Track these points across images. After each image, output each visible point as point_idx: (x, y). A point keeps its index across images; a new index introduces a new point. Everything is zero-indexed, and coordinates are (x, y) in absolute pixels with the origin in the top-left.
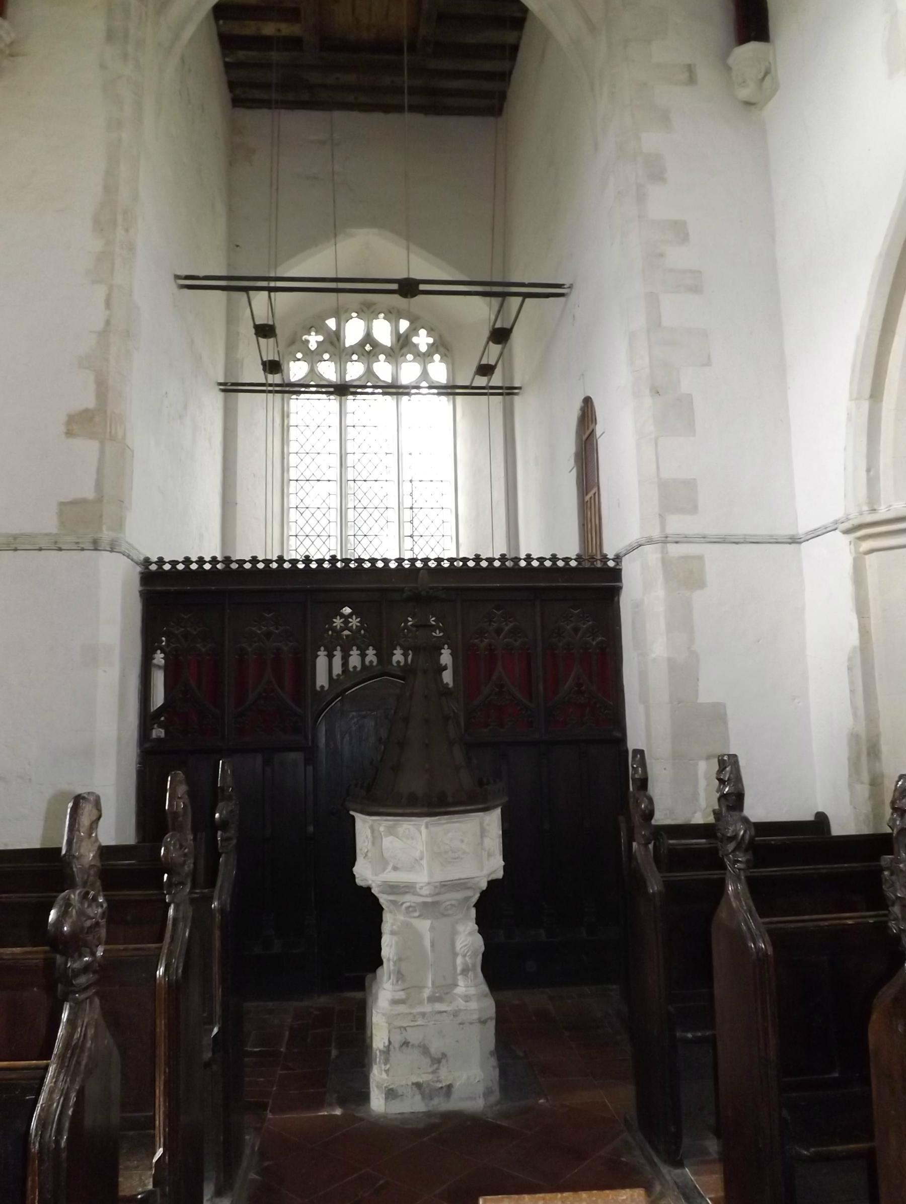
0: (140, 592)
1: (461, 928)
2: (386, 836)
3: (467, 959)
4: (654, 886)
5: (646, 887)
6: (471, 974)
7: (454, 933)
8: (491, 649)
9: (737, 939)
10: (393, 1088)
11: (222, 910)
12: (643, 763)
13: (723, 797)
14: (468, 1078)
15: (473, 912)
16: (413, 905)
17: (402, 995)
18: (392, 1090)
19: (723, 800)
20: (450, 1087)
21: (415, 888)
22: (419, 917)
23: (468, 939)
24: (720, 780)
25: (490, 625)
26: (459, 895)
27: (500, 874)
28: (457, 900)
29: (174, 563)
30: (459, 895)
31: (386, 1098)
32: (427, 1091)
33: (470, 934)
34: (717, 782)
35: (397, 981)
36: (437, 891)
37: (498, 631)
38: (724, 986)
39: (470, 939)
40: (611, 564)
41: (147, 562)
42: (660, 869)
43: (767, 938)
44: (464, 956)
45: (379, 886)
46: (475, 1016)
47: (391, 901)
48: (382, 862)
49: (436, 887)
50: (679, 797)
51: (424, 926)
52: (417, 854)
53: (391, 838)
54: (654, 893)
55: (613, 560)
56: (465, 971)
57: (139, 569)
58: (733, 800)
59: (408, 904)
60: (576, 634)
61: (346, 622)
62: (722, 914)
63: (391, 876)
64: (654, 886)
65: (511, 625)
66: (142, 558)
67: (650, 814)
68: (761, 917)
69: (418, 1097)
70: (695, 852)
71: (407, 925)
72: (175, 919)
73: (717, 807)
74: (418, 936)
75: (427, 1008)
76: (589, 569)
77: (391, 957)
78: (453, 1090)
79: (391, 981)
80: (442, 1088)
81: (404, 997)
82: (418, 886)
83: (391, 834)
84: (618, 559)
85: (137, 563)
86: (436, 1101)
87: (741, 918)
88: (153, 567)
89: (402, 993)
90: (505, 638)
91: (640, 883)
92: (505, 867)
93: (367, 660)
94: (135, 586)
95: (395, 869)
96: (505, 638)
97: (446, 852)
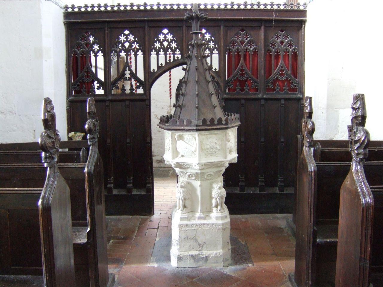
0: (64, 22)
1: (215, 186)
2: (178, 140)
3: (218, 200)
4: (312, 167)
5: (307, 169)
6: (219, 207)
7: (211, 188)
8: (238, 51)
9: (355, 195)
10: (177, 258)
11: (89, 173)
12: (310, 104)
13: (355, 118)
14: (216, 254)
15: (221, 178)
16: (191, 174)
17: (186, 215)
18: (180, 257)
19: (354, 120)
20: (207, 257)
21: (192, 165)
22: (195, 179)
23: (218, 190)
24: (353, 108)
25: (238, 39)
26: (215, 170)
27: (236, 161)
28: (214, 172)
29: (80, 8)
30: (215, 170)
31: (178, 261)
32: (196, 258)
33: (220, 188)
34: (352, 110)
35: (183, 209)
36: (203, 167)
37: (242, 42)
38: (345, 217)
39: (219, 191)
40: (302, 8)
41: (66, 7)
42: (316, 161)
43: (372, 196)
44: (216, 199)
45: (174, 164)
46: (221, 227)
47: (181, 172)
48: (176, 153)
49: (202, 165)
50: (329, 123)
51: (197, 184)
52: (193, 150)
53: (181, 141)
54: (312, 171)
55: (303, 5)
56: (216, 206)
57: (63, 11)
58: (360, 120)
59: (189, 174)
60: (282, 45)
61: (165, 37)
62: (347, 182)
63: (180, 160)
64: (312, 167)
65: (249, 39)
66: (64, 6)
67: (312, 131)
68: (369, 185)
69: (192, 261)
70: (334, 155)
71: (189, 183)
72: (49, 175)
73: (350, 124)
74: (193, 189)
75: (198, 222)
76: (290, 10)
77: (181, 198)
78: (208, 258)
79: (181, 209)
80: (204, 257)
81: (186, 216)
82: (193, 165)
83: (181, 139)
84: (305, 5)
85: (61, 8)
86: (200, 263)
87: (358, 185)
88: (70, 10)
89: (186, 214)
90: (245, 46)
91: (304, 166)
92: (238, 157)
93: (176, 56)
94: (61, 19)
95: (183, 156)
96: (245, 46)
97: (208, 149)
